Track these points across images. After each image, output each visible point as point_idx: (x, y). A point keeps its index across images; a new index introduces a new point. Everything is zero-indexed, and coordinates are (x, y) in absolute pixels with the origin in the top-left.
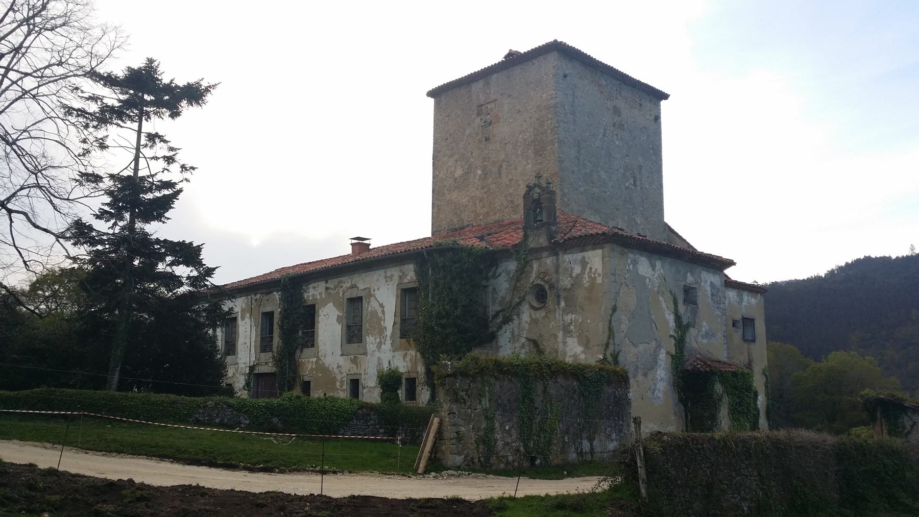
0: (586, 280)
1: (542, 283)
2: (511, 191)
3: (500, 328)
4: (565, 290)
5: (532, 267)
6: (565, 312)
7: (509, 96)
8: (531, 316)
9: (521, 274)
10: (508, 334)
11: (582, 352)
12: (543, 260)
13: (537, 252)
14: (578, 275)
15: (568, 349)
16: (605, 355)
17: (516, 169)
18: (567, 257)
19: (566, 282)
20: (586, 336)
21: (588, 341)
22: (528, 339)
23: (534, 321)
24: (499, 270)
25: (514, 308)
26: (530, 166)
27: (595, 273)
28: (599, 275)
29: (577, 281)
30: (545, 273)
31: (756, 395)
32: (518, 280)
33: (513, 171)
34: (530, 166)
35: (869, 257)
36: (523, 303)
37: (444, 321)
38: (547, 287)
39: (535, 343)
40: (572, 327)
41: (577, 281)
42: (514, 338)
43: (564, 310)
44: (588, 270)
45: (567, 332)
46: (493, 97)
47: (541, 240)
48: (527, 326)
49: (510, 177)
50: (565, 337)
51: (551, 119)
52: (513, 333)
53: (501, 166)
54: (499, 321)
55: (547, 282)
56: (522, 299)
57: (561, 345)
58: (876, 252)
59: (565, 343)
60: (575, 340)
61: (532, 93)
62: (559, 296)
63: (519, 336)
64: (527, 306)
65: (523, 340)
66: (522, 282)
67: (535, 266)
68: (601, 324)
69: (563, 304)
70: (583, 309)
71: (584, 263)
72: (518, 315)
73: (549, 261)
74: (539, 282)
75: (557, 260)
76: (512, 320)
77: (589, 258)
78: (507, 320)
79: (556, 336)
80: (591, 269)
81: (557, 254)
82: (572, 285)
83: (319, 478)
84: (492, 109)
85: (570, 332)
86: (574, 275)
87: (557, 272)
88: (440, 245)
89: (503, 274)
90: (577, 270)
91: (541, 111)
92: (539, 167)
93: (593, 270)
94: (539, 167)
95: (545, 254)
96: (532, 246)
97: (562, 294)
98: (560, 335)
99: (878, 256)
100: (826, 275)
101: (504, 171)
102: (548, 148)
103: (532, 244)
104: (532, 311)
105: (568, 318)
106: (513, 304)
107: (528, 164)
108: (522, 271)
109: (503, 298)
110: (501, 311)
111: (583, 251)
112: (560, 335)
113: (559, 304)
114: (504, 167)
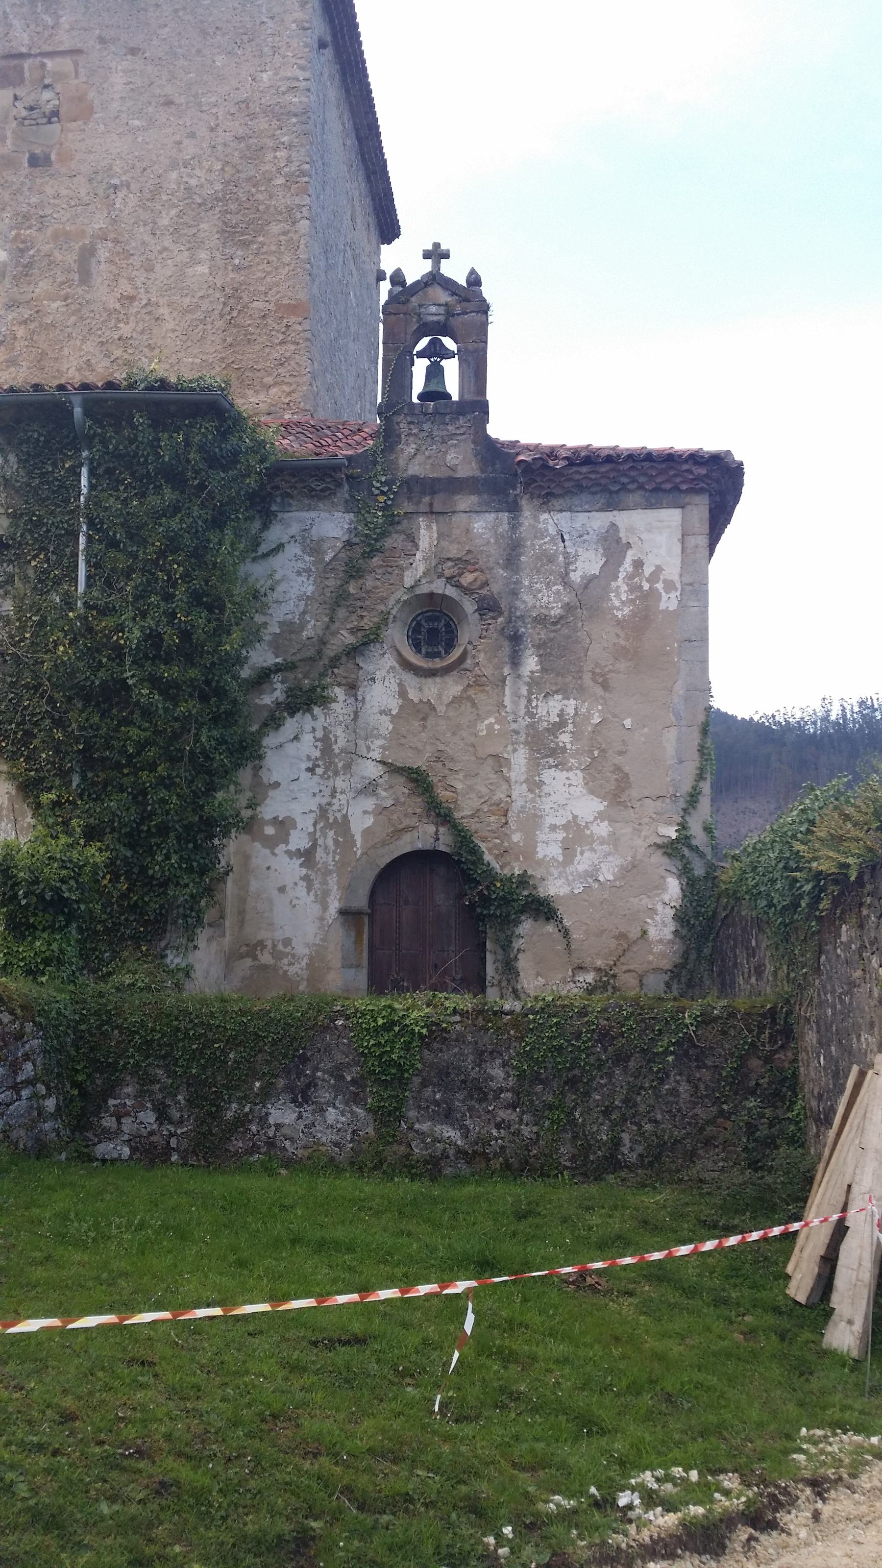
0: (619, 598)
1: (451, 591)
2: (126, 330)
3: (273, 722)
4: (541, 620)
5: (413, 539)
6: (538, 686)
7: (133, 51)
8: (403, 693)
9: (368, 555)
10: (308, 746)
11: (600, 816)
12: (459, 519)
13: (436, 491)
14: (589, 581)
15: (546, 805)
16: (683, 826)
17: (150, 269)
18: (551, 522)
19: (542, 597)
20: (618, 769)
21: (623, 782)
22: (393, 769)
23: (418, 712)
24: (275, 534)
25: (335, 662)
26: (203, 269)
27: (653, 578)
28: (669, 586)
29: (587, 599)
30: (464, 563)
32: (354, 572)
33: (141, 277)
34: (203, 269)
36: (375, 650)
37: (170, 672)
38: (469, 606)
39: (418, 780)
40: (565, 738)
41: (587, 599)
43: (534, 683)
44: (627, 566)
45: (544, 747)
46: (65, 41)
47: (453, 457)
48: (386, 725)
49: (125, 287)
50: (535, 765)
51: (290, 147)
52: (326, 742)
53: (87, 254)
54: (267, 700)
55: (467, 591)
56: (368, 640)
57: (519, 792)
59: (535, 785)
60: (577, 777)
61: (220, 61)
62: (516, 639)
63: (353, 755)
64: (389, 661)
65: (372, 770)
66: (369, 583)
67: (427, 535)
68: (671, 736)
69: (531, 663)
70: (605, 686)
71: (613, 546)
72: (352, 687)
73: (483, 527)
74: (439, 587)
75: (514, 527)
76: (325, 701)
77: (631, 530)
78: (304, 700)
79: (500, 763)
80: (638, 564)
81: (514, 508)
82: (568, 607)
84: (60, 76)
85: (556, 752)
86: (575, 577)
87: (511, 561)
88: (163, 384)
89: (293, 549)
90: (589, 563)
91: (252, 116)
92: (239, 277)
93: (648, 570)
94: (239, 277)
95: (465, 502)
96: (415, 469)
97: (532, 633)
98: (519, 759)
101: (101, 270)
102: (275, 228)
104: (410, 680)
105: (550, 708)
106: (330, 651)
107: (195, 261)
108: (368, 548)
109: (290, 628)
110: (277, 669)
111: (611, 506)
112: (519, 759)
113: (515, 661)
114: (103, 253)
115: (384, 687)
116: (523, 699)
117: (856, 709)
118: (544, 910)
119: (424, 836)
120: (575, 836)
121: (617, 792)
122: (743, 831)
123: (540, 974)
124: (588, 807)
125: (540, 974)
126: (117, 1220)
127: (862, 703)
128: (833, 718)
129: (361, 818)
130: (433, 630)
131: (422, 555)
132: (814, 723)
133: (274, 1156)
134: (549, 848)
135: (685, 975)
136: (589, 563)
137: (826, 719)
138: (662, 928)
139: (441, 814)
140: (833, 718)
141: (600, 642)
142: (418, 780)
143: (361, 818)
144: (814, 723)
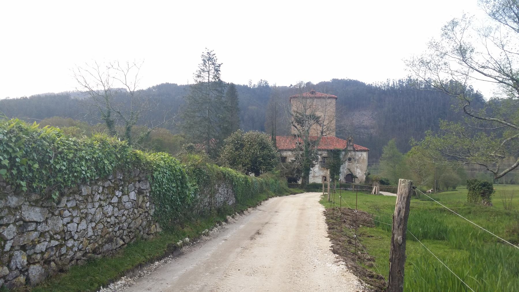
0: (362, 158)
13: (350, 151)
19: (357, 158)
23: (349, 165)
29: (360, 158)
31: (143, 150)
35: (176, 84)
39: (349, 169)
41: (360, 158)
42: (343, 168)
45: (357, 167)
56: (346, 160)
58: (171, 81)
67: (349, 153)
71: (362, 155)
73: (353, 153)
83: (355, 194)
90: (360, 156)
99: (11, 98)
100: (30, 97)
103: (349, 149)
108: (346, 154)
115: (347, 163)
116: (356, 164)
117: (398, 83)
118: (357, 178)
119: (349, 173)
120: (359, 173)
121: (361, 170)
122: (361, 121)
123: (357, 182)
124: (360, 171)
125: (357, 182)
126: (120, 256)
127: (399, 81)
128: (390, 85)
129: (345, 172)
130: (350, 159)
131: (349, 155)
132: (385, 87)
133: (348, 190)
134: (357, 174)
135: (366, 182)
136: (360, 156)
137: (388, 86)
138: (364, 179)
139: (350, 171)
140: (390, 85)
141: (361, 161)
142: (349, 169)
143: (345, 172)
144: (385, 87)
